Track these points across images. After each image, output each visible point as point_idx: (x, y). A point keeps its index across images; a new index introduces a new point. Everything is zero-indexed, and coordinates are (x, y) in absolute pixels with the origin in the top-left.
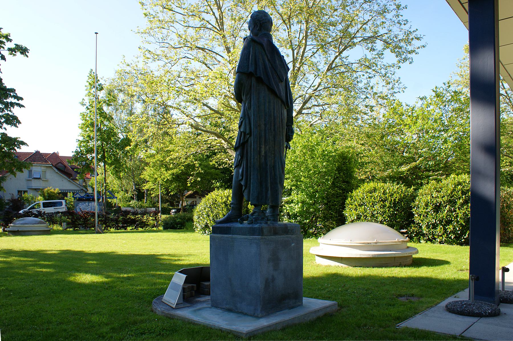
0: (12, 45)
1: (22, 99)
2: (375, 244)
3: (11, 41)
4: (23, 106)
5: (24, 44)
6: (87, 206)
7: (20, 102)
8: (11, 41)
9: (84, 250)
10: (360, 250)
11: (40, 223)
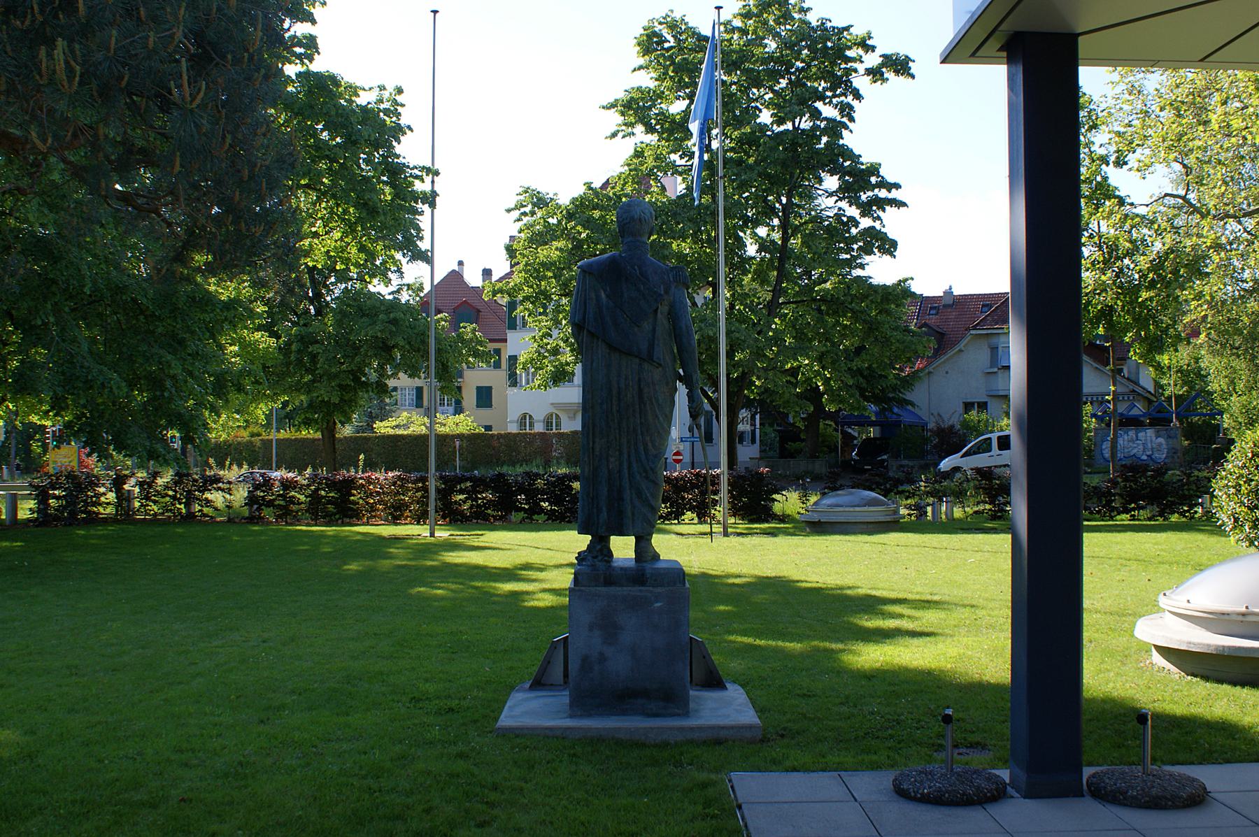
0: (872, 60)
1: (897, 186)
2: (1241, 618)
3: (873, 48)
4: (904, 204)
5: (903, 51)
6: (1132, 441)
7: (894, 194)
8: (873, 48)
9: (847, 581)
10: (1208, 629)
11: (874, 503)
